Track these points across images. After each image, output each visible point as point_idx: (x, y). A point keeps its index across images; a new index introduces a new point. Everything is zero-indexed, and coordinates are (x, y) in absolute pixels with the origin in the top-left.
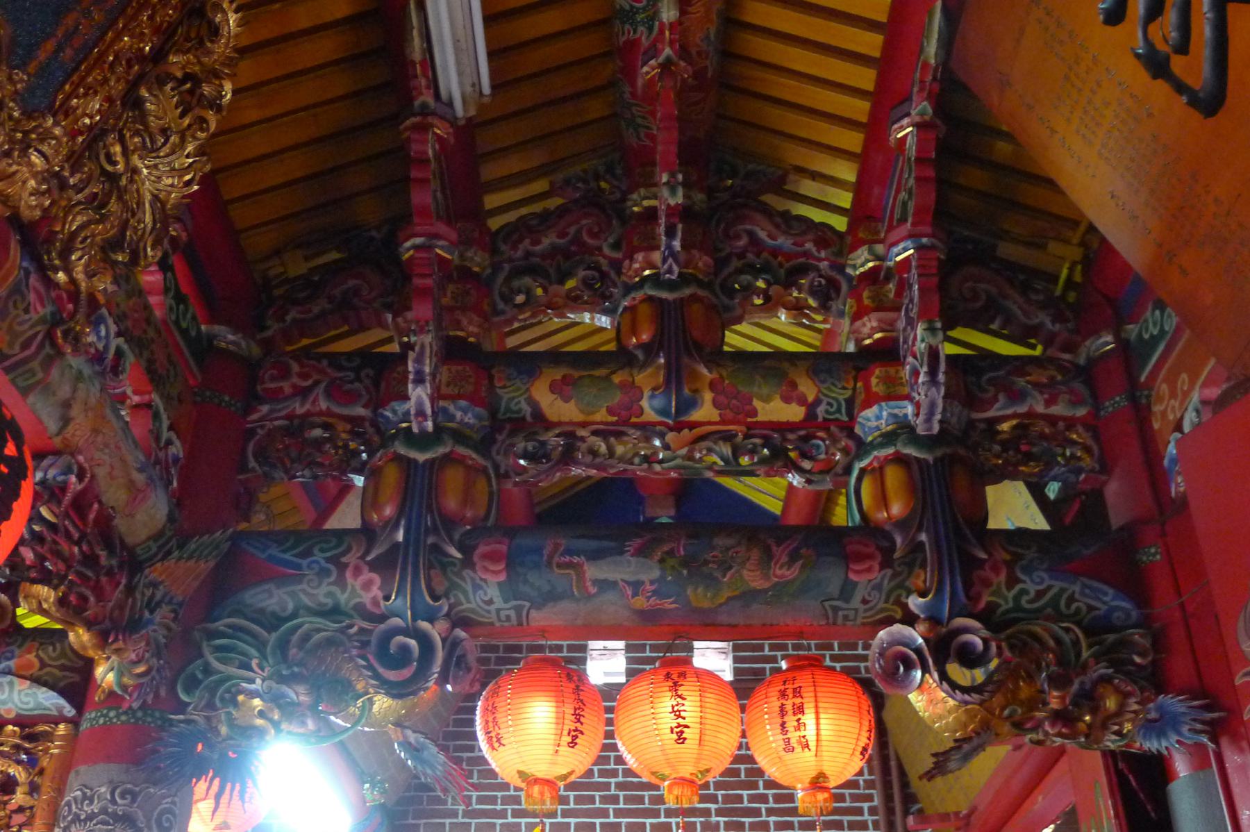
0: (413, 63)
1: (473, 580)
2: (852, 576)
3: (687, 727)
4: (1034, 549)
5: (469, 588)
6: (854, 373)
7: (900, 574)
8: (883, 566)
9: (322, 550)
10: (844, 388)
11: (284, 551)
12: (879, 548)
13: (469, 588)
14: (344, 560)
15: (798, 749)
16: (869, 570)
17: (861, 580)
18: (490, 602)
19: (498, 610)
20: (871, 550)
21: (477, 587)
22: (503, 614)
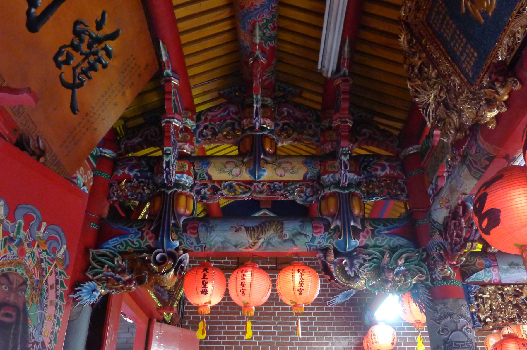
0: (164, 62)
1: (186, 236)
2: (315, 235)
3: (303, 290)
4: (382, 225)
5: (185, 239)
6: (319, 163)
7: (331, 233)
8: (325, 230)
9: (136, 226)
10: (316, 168)
11: (125, 226)
12: (324, 225)
13: (185, 239)
14: (143, 229)
16: (320, 232)
17: (318, 236)
18: (192, 244)
19: (195, 247)
20: (322, 225)
21: (187, 239)
22: (196, 248)
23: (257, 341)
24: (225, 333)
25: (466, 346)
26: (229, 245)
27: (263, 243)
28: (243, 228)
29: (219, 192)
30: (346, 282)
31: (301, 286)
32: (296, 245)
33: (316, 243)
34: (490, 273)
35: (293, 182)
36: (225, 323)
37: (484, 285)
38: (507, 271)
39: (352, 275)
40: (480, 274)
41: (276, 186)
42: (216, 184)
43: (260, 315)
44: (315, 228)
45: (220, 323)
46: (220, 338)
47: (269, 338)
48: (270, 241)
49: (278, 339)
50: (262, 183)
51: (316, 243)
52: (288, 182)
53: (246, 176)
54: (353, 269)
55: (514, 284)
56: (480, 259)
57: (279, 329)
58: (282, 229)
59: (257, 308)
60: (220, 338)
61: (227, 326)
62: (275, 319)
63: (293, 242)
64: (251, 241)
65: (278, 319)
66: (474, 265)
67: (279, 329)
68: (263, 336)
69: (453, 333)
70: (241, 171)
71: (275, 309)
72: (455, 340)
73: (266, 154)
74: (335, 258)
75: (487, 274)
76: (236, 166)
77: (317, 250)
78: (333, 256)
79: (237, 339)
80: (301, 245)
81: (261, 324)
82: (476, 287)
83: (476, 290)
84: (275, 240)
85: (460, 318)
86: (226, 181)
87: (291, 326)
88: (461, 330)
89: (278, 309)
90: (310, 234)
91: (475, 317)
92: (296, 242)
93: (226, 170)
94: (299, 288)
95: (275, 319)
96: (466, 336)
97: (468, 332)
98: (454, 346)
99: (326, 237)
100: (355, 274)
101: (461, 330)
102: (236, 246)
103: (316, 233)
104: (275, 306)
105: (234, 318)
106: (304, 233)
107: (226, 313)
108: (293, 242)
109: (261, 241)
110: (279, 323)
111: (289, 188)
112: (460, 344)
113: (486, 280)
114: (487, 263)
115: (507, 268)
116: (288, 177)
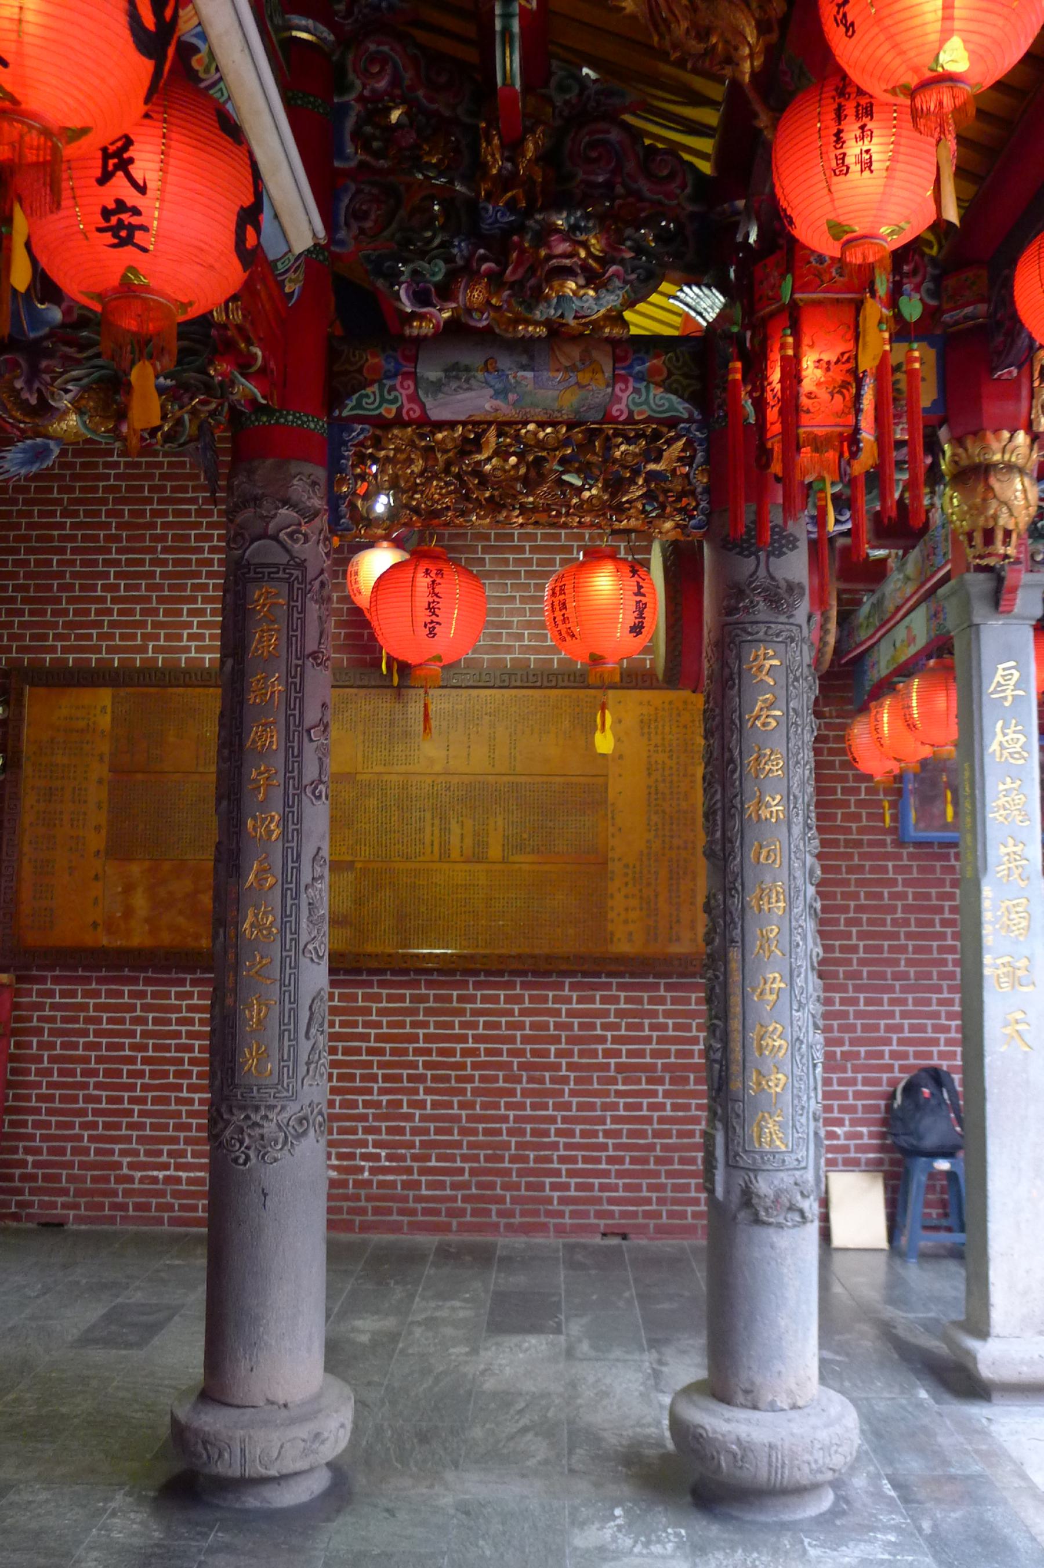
15: (568, 638)
23: (109, 595)
24: (28, 576)
25: (281, 575)
34: (393, 393)
36: (74, 550)
37: (383, 424)
38: (437, 387)
39: (33, 401)
40: (367, 396)
43: (117, 528)
46: (17, 588)
47: (138, 587)
49: (159, 587)
54: (36, 385)
55: (464, 424)
56: (374, 355)
57: (164, 563)
60: (17, 588)
61: (32, 557)
62: (155, 538)
65: (163, 538)
66: (360, 371)
67: (164, 563)
68: (122, 583)
69: (256, 544)
71: (155, 513)
72: (256, 560)
75: (387, 396)
79: (58, 591)
81: (119, 551)
82: (362, 430)
83: (362, 437)
85: (277, 508)
87: (194, 557)
88: (275, 538)
89: (164, 513)
91: (343, 508)
95: (155, 538)
96: (287, 550)
97: (296, 541)
98: (252, 575)
100: (42, 398)
101: (275, 538)
104: (155, 506)
105: (51, 538)
107: (31, 526)
110: (165, 550)
112: (266, 570)
113: (389, 411)
114: (391, 366)
115: (440, 380)
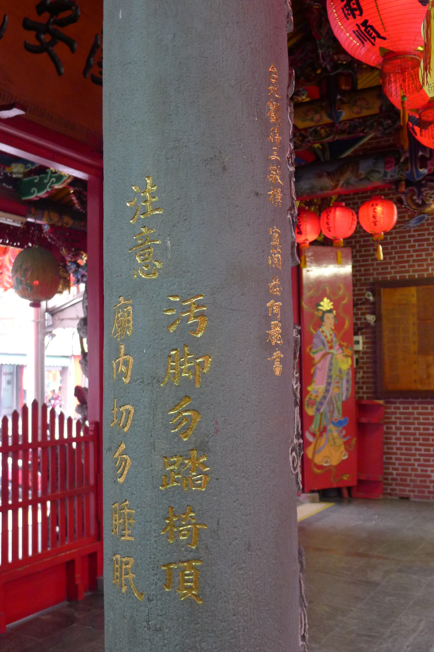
16: (391, 167)
17: (389, 171)
26: (315, 190)
27: (343, 184)
28: (325, 174)
29: (306, 140)
30: (417, 208)
31: (375, 218)
32: (371, 182)
33: (389, 177)
35: (372, 116)
41: (356, 123)
42: (303, 132)
44: (386, 163)
45: (409, 242)
48: (348, 180)
50: (343, 123)
51: (389, 177)
52: (367, 117)
53: (326, 120)
58: (358, 169)
59: (386, 233)
63: (369, 179)
64: (333, 184)
70: (321, 117)
73: (343, 93)
74: (406, 188)
76: (316, 112)
77: (391, 182)
78: (404, 187)
80: (376, 180)
84: (353, 180)
86: (311, 128)
90: (382, 170)
92: (372, 179)
93: (308, 118)
94: (373, 220)
99: (397, 170)
102: (322, 189)
103: (388, 168)
106: (377, 169)
108: (369, 179)
109: (341, 183)
111: (368, 123)
116: (365, 113)
